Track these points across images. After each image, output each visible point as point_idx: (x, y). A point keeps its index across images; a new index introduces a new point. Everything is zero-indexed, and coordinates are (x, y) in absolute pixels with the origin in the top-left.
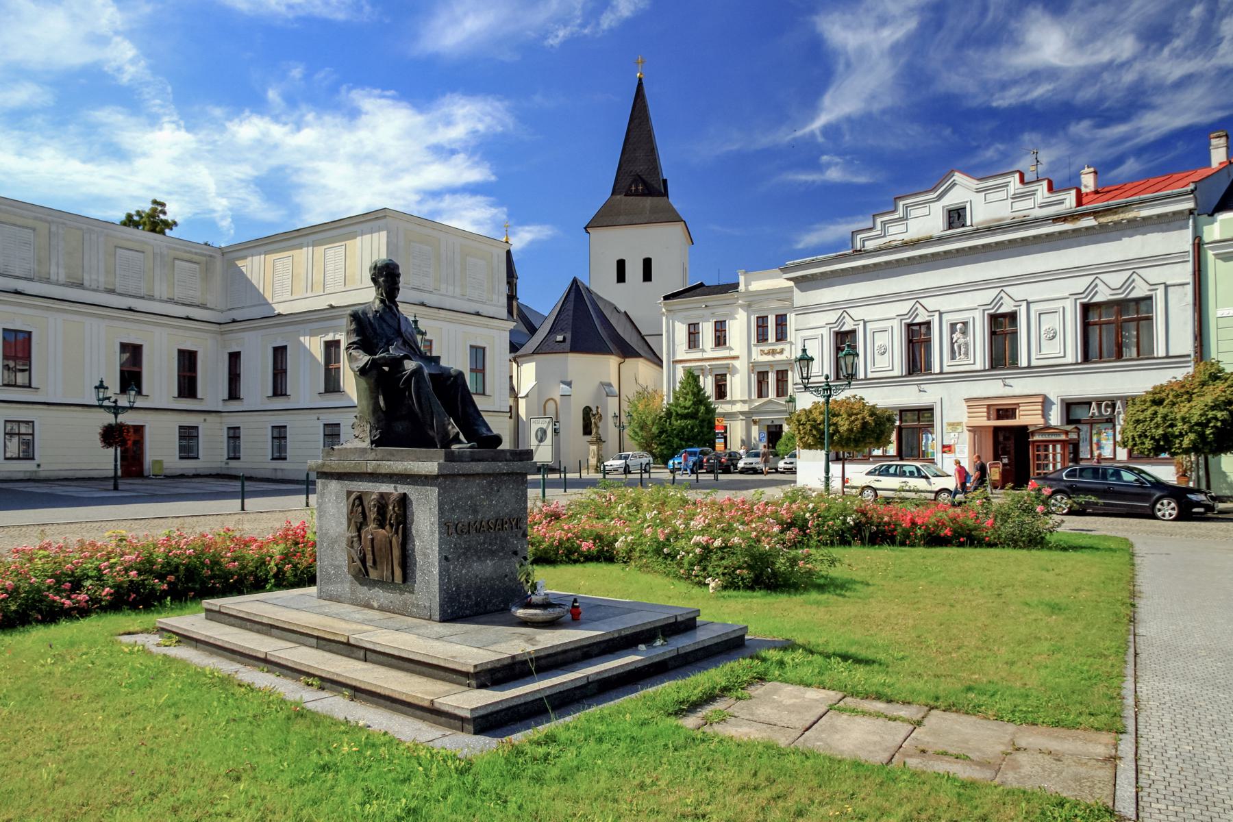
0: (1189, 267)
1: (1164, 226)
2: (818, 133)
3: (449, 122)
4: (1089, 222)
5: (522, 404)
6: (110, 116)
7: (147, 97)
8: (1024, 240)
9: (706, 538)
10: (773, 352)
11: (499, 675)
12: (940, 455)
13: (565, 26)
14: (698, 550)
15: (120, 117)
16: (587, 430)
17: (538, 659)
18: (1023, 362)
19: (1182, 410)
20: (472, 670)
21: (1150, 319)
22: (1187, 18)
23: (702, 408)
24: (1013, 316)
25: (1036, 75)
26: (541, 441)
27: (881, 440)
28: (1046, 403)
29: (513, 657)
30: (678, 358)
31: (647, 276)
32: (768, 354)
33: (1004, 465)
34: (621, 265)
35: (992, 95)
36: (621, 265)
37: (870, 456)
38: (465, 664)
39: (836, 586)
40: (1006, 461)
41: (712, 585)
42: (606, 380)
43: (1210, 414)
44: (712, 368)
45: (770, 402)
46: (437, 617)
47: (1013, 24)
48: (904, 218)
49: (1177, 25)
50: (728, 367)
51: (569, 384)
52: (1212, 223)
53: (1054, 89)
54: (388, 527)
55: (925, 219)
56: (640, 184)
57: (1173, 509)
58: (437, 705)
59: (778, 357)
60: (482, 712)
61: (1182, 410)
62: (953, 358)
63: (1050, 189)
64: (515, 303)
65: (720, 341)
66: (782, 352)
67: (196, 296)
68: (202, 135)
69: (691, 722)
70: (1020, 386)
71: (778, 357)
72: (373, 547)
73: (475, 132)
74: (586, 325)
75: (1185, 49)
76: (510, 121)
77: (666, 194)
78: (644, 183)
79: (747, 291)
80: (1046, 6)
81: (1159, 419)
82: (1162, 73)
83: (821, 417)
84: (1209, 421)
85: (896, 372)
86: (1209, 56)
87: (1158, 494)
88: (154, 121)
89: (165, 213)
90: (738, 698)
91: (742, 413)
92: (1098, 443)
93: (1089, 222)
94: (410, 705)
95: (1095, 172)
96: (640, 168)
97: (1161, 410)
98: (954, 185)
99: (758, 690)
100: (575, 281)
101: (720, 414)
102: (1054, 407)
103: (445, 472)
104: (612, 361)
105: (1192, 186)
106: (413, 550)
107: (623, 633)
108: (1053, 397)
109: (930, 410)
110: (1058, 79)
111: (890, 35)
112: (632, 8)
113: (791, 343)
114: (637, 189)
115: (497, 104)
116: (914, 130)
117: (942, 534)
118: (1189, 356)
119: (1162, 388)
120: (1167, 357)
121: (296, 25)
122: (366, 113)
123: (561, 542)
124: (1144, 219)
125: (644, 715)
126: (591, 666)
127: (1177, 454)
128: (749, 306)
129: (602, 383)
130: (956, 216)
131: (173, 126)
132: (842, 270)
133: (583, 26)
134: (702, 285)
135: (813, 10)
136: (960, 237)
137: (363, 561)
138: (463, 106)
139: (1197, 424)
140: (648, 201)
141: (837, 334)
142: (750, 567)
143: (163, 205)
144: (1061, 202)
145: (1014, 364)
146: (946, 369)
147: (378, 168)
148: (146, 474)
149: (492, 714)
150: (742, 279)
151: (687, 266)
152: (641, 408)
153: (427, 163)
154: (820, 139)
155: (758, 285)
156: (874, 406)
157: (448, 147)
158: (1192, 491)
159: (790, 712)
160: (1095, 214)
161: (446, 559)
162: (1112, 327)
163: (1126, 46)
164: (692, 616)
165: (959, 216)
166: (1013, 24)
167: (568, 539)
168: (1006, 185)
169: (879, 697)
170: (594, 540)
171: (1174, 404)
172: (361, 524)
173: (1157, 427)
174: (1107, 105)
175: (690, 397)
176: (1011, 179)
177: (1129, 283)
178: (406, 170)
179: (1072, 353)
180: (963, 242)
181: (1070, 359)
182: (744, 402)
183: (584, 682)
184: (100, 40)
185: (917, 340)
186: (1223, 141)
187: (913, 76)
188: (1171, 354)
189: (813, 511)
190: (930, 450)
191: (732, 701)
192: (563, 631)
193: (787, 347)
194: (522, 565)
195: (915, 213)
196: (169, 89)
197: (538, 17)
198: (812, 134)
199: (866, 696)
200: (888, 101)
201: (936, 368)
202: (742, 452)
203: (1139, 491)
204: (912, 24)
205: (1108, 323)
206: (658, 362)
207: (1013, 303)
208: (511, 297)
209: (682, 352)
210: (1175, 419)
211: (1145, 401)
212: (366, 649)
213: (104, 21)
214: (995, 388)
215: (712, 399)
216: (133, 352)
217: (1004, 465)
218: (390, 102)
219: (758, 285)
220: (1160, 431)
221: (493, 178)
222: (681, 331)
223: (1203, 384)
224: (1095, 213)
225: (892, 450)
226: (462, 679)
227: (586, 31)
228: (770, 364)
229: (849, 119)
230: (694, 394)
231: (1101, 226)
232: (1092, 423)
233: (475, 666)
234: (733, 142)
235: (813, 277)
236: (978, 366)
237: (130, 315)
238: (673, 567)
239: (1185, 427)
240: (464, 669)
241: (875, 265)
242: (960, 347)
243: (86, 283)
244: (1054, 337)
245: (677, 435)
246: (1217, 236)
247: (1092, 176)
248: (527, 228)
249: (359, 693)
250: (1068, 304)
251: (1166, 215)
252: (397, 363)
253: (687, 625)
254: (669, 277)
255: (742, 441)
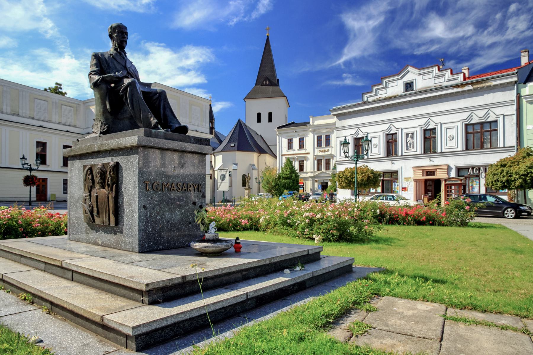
0: (515, 107)
1: (503, 89)
2: (342, 64)
3: (187, 57)
4: (469, 87)
5: (216, 172)
6: (42, 52)
7: (58, 44)
8: (439, 96)
9: (311, 214)
10: (324, 151)
11: (171, 293)
12: (401, 192)
13: (237, 17)
14: (307, 221)
15: (47, 53)
16: (244, 184)
17: (206, 279)
18: (439, 150)
19: (515, 169)
20: (144, 289)
21: (497, 130)
22: (494, 19)
23: (294, 175)
24: (433, 131)
25: (432, 41)
26: (223, 180)
27: (375, 185)
28: (449, 168)
29: (184, 277)
30: (283, 153)
31: (270, 120)
32: (322, 152)
33: (429, 196)
34: (259, 115)
35: (414, 49)
36: (259, 115)
37: (369, 192)
38: (139, 283)
39: (384, 241)
40: (430, 195)
41: (317, 239)
42: (252, 163)
43: (529, 171)
44: (298, 158)
45: (323, 172)
46: (137, 249)
47: (424, 20)
48: (386, 87)
49: (490, 21)
50: (305, 157)
51: (236, 164)
52: (525, 87)
53: (440, 47)
54: (106, 187)
55: (395, 87)
56: (267, 80)
57: (513, 213)
58: (106, 321)
59: (326, 153)
60: (145, 330)
61: (515, 169)
62: (407, 149)
63: (452, 73)
64: (213, 131)
65: (302, 146)
66: (328, 151)
67: (72, 122)
68: (82, 61)
69: (338, 334)
70: (437, 161)
71: (326, 153)
72: (97, 202)
73: (198, 62)
74: (243, 140)
75: (493, 32)
76: (213, 57)
77: (278, 85)
78: (269, 81)
79: (313, 125)
80: (437, 13)
81: (505, 173)
82: (484, 42)
83: (349, 174)
84: (528, 174)
85: (382, 156)
86: (503, 34)
87: (506, 207)
88: (61, 55)
89: (61, 89)
90: (368, 311)
91: (310, 177)
92: (472, 186)
93: (469, 87)
94: (87, 319)
95: (468, 69)
96: (268, 74)
97: (505, 169)
98: (408, 72)
99: (379, 303)
100: (239, 121)
101: (301, 178)
102: (452, 170)
103: (144, 143)
104: (255, 155)
105: (516, 71)
106: (123, 202)
107: (273, 261)
108: (452, 166)
109: (396, 172)
110: (442, 43)
111: (372, 23)
112: (265, 10)
113: (332, 147)
114: (266, 83)
115: (208, 50)
116: (382, 64)
117: (421, 219)
118: (514, 147)
119: (505, 160)
120: (504, 147)
121: (122, 15)
122: (152, 53)
123: (230, 221)
124: (494, 86)
125: (298, 330)
126: (250, 285)
127: (513, 189)
128: (314, 131)
129: (251, 165)
130: (409, 86)
131: (70, 57)
132: (358, 110)
133: (244, 17)
134: (294, 123)
135: (340, 12)
136: (410, 95)
137: (92, 212)
138: (193, 51)
139: (523, 175)
140: (271, 88)
141: (355, 139)
142: (338, 229)
143: (60, 85)
144: (456, 79)
145: (435, 152)
146: (404, 154)
147: (157, 76)
148: (48, 200)
149: (156, 330)
150: (311, 120)
151: (287, 116)
152: (267, 174)
153: (178, 75)
154: (343, 67)
155: (317, 122)
156: (372, 170)
157: (187, 68)
158: (522, 205)
159: (417, 323)
160: (472, 84)
161: (144, 207)
162: (480, 135)
163: (470, 30)
164: (318, 250)
165: (410, 86)
166: (424, 20)
167: (234, 219)
168: (432, 72)
169: (474, 308)
170: (248, 220)
171: (511, 167)
172: (91, 187)
173: (504, 177)
174: (461, 54)
175: (289, 170)
176: (434, 69)
177: (487, 114)
178: (169, 78)
179: (461, 146)
180: (412, 97)
181: (460, 149)
182: (312, 172)
183: (244, 298)
184: (38, 19)
185: (391, 142)
186: (526, 53)
187: (382, 41)
188: (506, 146)
189: (358, 208)
190: (396, 190)
191: (364, 313)
192: (228, 259)
193: (330, 149)
194: (199, 212)
195: (390, 85)
196: (68, 41)
197: (226, 12)
198: (339, 65)
199: (463, 308)
200: (371, 51)
201: (399, 154)
202: (311, 193)
203: (498, 205)
204: (382, 19)
205: (477, 133)
206: (275, 157)
207: (434, 124)
208: (212, 128)
209: (285, 151)
210: (512, 173)
211: (497, 166)
212: (73, 271)
213: (39, 11)
214: (425, 162)
215: (298, 171)
216: (42, 145)
217: (429, 196)
218: (162, 48)
219: (319, 122)
220: (505, 178)
221: (206, 82)
222: (285, 142)
223: (524, 158)
224: (472, 83)
225: (379, 189)
226: (138, 296)
227: (246, 19)
228: (323, 156)
229: (355, 59)
230: (290, 169)
231: (475, 89)
232: (469, 177)
233: (147, 285)
234: (307, 68)
235: (345, 114)
236: (419, 152)
237: (41, 129)
238: (291, 230)
239: (517, 176)
240: (138, 287)
241: (372, 108)
242: (410, 144)
243: (20, 114)
244: (453, 139)
245: (283, 186)
246: (527, 93)
247: (467, 70)
248: (220, 103)
249: (55, 308)
250: (459, 124)
251: (504, 84)
252: (119, 81)
253: (312, 258)
254: (279, 119)
255: (311, 189)
